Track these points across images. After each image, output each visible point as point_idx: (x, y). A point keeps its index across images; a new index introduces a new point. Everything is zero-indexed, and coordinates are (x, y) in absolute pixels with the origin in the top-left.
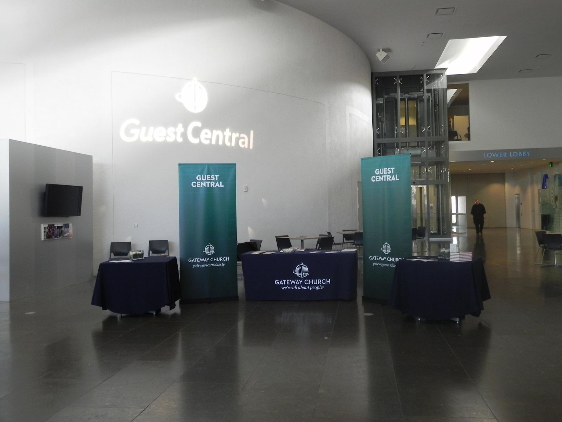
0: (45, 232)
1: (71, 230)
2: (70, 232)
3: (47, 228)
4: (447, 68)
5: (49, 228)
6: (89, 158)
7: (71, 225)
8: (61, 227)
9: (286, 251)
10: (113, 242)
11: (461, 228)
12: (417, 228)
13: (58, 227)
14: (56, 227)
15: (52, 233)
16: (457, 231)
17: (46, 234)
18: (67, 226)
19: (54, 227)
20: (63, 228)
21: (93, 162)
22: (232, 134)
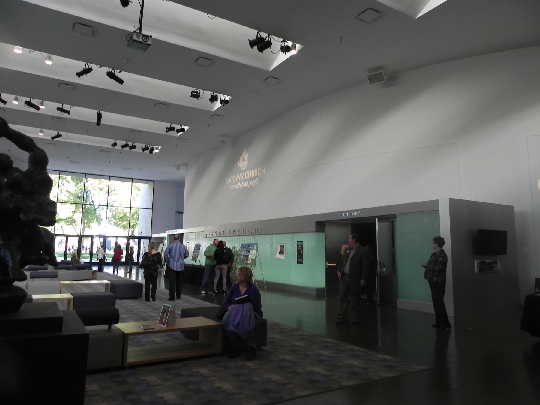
0: (478, 267)
1: (499, 266)
2: (498, 267)
3: (480, 263)
4: (127, 212)
5: (481, 263)
6: (512, 207)
7: (498, 262)
8: (491, 263)
9: (160, 278)
10: (537, 277)
11: (141, 272)
12: (75, 270)
13: (488, 263)
14: (487, 263)
15: (483, 267)
16: (105, 272)
17: (479, 268)
18: (496, 262)
19: (486, 263)
20: (492, 265)
21: (515, 211)
22: (151, 235)
